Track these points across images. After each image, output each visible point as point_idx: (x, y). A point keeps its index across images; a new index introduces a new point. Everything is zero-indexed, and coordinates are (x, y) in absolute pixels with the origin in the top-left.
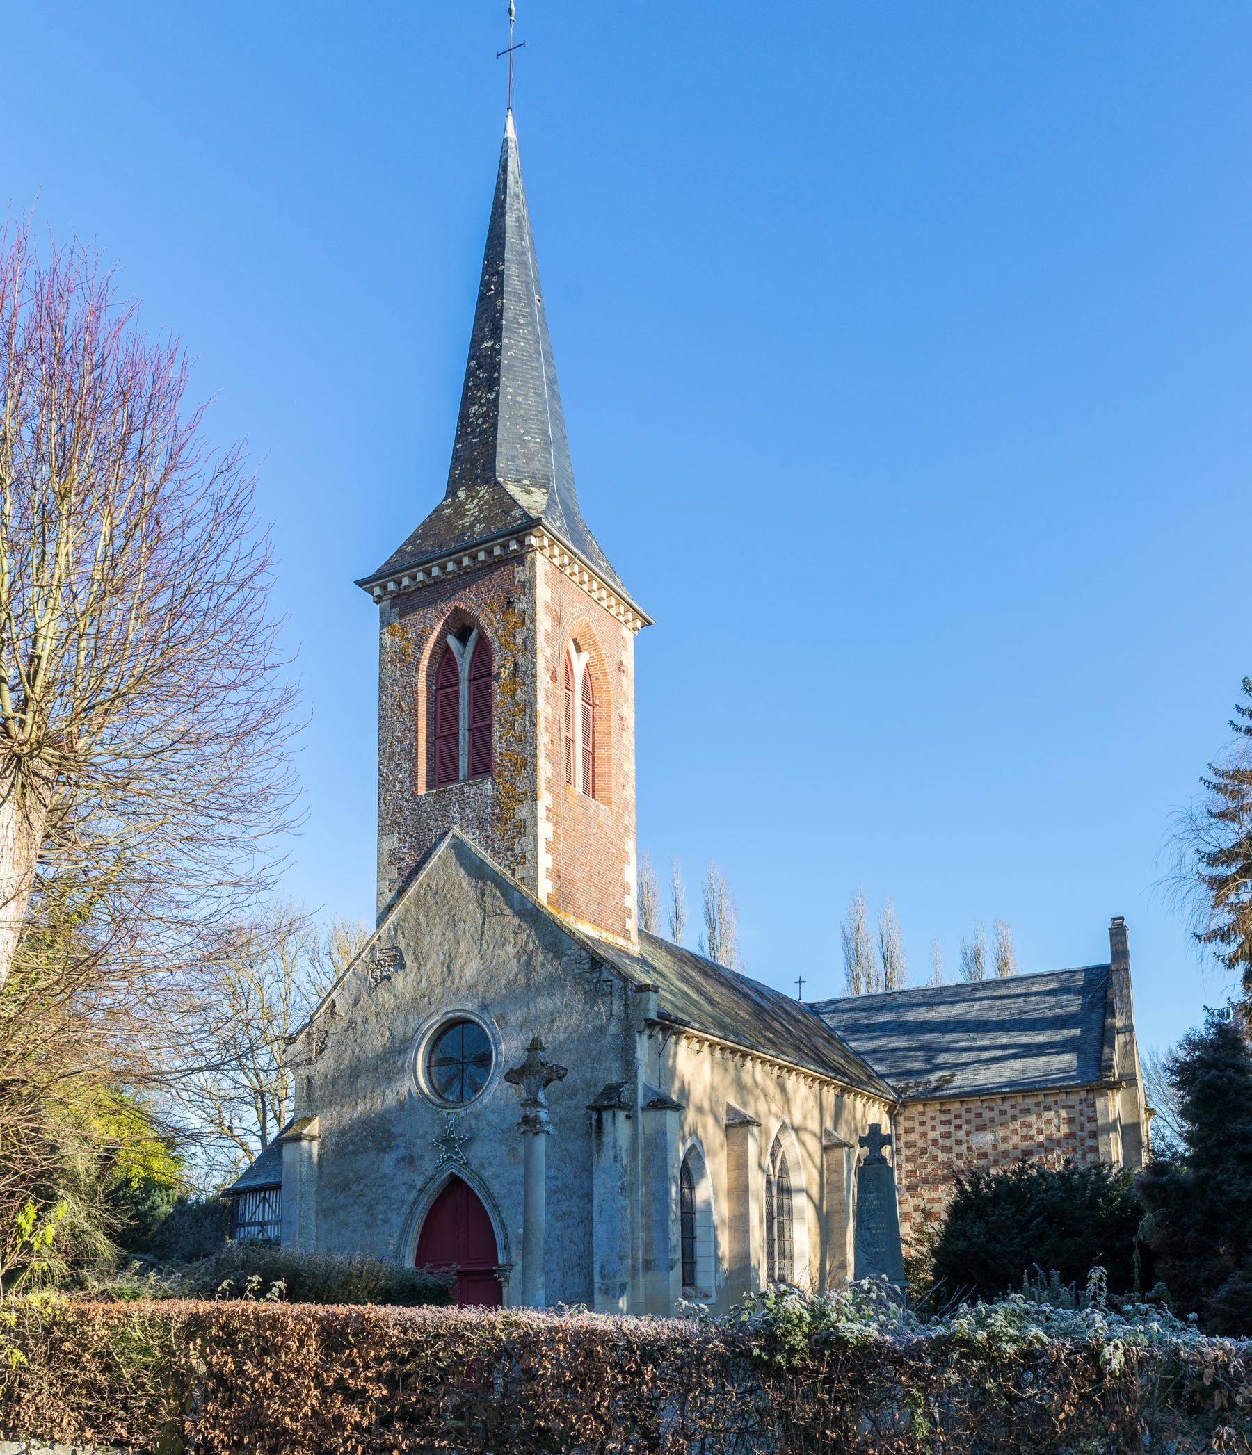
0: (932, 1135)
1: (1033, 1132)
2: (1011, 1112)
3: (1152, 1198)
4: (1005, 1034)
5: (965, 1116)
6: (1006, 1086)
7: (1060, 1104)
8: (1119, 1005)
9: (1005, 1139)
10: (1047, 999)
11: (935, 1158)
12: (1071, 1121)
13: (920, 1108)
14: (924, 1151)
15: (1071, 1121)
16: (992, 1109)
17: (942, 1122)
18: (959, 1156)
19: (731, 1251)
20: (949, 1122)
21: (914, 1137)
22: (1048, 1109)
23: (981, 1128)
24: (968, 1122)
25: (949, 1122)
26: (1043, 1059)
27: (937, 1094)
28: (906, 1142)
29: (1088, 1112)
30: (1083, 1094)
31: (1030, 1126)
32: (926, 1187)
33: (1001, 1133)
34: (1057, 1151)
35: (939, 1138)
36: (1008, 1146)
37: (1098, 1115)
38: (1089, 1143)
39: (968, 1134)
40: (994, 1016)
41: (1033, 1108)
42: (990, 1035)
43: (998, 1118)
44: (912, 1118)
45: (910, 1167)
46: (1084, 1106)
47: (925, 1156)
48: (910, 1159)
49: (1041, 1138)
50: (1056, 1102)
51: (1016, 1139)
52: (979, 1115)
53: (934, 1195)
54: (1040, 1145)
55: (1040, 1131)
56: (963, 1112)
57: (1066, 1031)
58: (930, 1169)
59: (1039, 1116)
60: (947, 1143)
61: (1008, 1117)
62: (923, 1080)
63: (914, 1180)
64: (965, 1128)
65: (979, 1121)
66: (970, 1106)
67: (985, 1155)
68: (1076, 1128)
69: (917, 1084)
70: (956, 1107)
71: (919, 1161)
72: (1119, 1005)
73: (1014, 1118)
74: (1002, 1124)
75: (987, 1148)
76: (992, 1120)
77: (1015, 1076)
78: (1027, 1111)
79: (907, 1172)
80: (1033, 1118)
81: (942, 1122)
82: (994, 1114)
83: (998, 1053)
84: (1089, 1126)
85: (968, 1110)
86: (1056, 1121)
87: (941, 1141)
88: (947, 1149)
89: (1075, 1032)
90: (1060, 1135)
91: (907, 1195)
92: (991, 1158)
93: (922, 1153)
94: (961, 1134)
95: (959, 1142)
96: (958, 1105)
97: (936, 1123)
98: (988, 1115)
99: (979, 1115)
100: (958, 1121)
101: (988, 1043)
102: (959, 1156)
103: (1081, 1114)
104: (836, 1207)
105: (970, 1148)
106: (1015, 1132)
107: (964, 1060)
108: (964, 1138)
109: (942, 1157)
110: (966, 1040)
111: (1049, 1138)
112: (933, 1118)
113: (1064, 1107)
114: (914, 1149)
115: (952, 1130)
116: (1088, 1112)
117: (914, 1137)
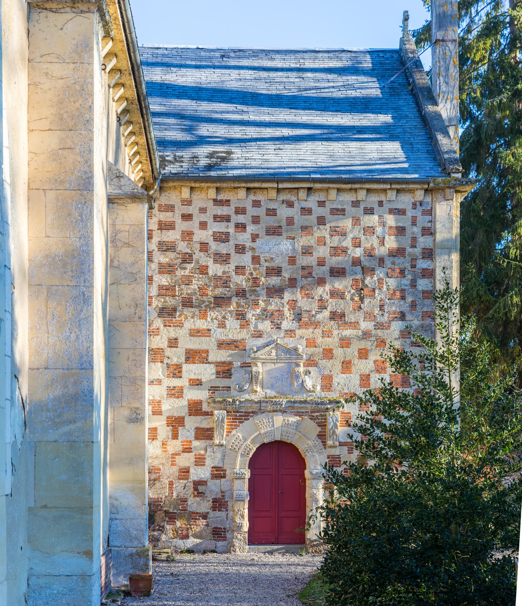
0: (200, 235)
1: (347, 243)
2: (318, 211)
3: (308, 366)
4: (288, 111)
5: (251, 211)
6: (315, 172)
7: (387, 206)
8: (444, 88)
9: (307, 251)
10: (331, 77)
11: (203, 270)
12: (400, 231)
13: (186, 193)
14: (187, 258)
15: (400, 231)
16: (290, 204)
17: (216, 218)
18: (240, 270)
19: (36, 352)
20: (227, 219)
21: (171, 236)
22: (369, 211)
23: (274, 231)
24: (256, 220)
25: (227, 219)
26: (354, 145)
27: (213, 174)
28: (161, 243)
29: (423, 221)
30: (419, 195)
31: (344, 234)
32: (188, 312)
33: (304, 241)
34: (380, 273)
35: (210, 241)
36: (311, 260)
37: (438, 226)
38: (422, 264)
39: (254, 237)
40: (262, 88)
41: (348, 208)
42: (265, 109)
43: (299, 220)
44: (170, 208)
45: (164, 280)
46: (418, 213)
47: (189, 266)
48: (167, 269)
49: (358, 252)
50: (381, 204)
51: (323, 252)
52: (271, 212)
53: (201, 324)
54: (356, 262)
55: (357, 244)
56: (248, 205)
57: (371, 116)
58: (194, 286)
59: (356, 221)
60: (223, 249)
61: (313, 219)
62: (186, 154)
63: (170, 302)
64: (251, 228)
65: (271, 221)
66: (260, 197)
67: (277, 271)
68: (406, 242)
69: (177, 160)
70: (239, 197)
71: (180, 273)
72: (444, 88)
73: (321, 221)
74: (304, 228)
75: (280, 261)
76: (290, 221)
77: (324, 161)
78: (340, 212)
79: (160, 287)
80: (347, 223)
81: (216, 218)
82: (294, 212)
83: (286, 132)
84: (424, 242)
85: (256, 204)
86: (379, 230)
87: (214, 246)
88: (222, 259)
89: (385, 118)
90: (382, 251)
91: (158, 323)
92: (286, 275)
93: (184, 261)
94: (244, 238)
95: (240, 249)
96: (242, 193)
97: (207, 217)
98: (284, 212)
99: (271, 212)
100: (241, 218)
101: (267, 118)
102: (240, 270)
103: (414, 223)
104: (126, 311)
105: (256, 260)
106: (322, 241)
107: (238, 136)
108: (248, 244)
109: (215, 269)
110: (233, 112)
111: (370, 254)
112: (203, 210)
113: (391, 211)
114: (171, 255)
115: (231, 230)
116: (423, 221)
117: (171, 236)
